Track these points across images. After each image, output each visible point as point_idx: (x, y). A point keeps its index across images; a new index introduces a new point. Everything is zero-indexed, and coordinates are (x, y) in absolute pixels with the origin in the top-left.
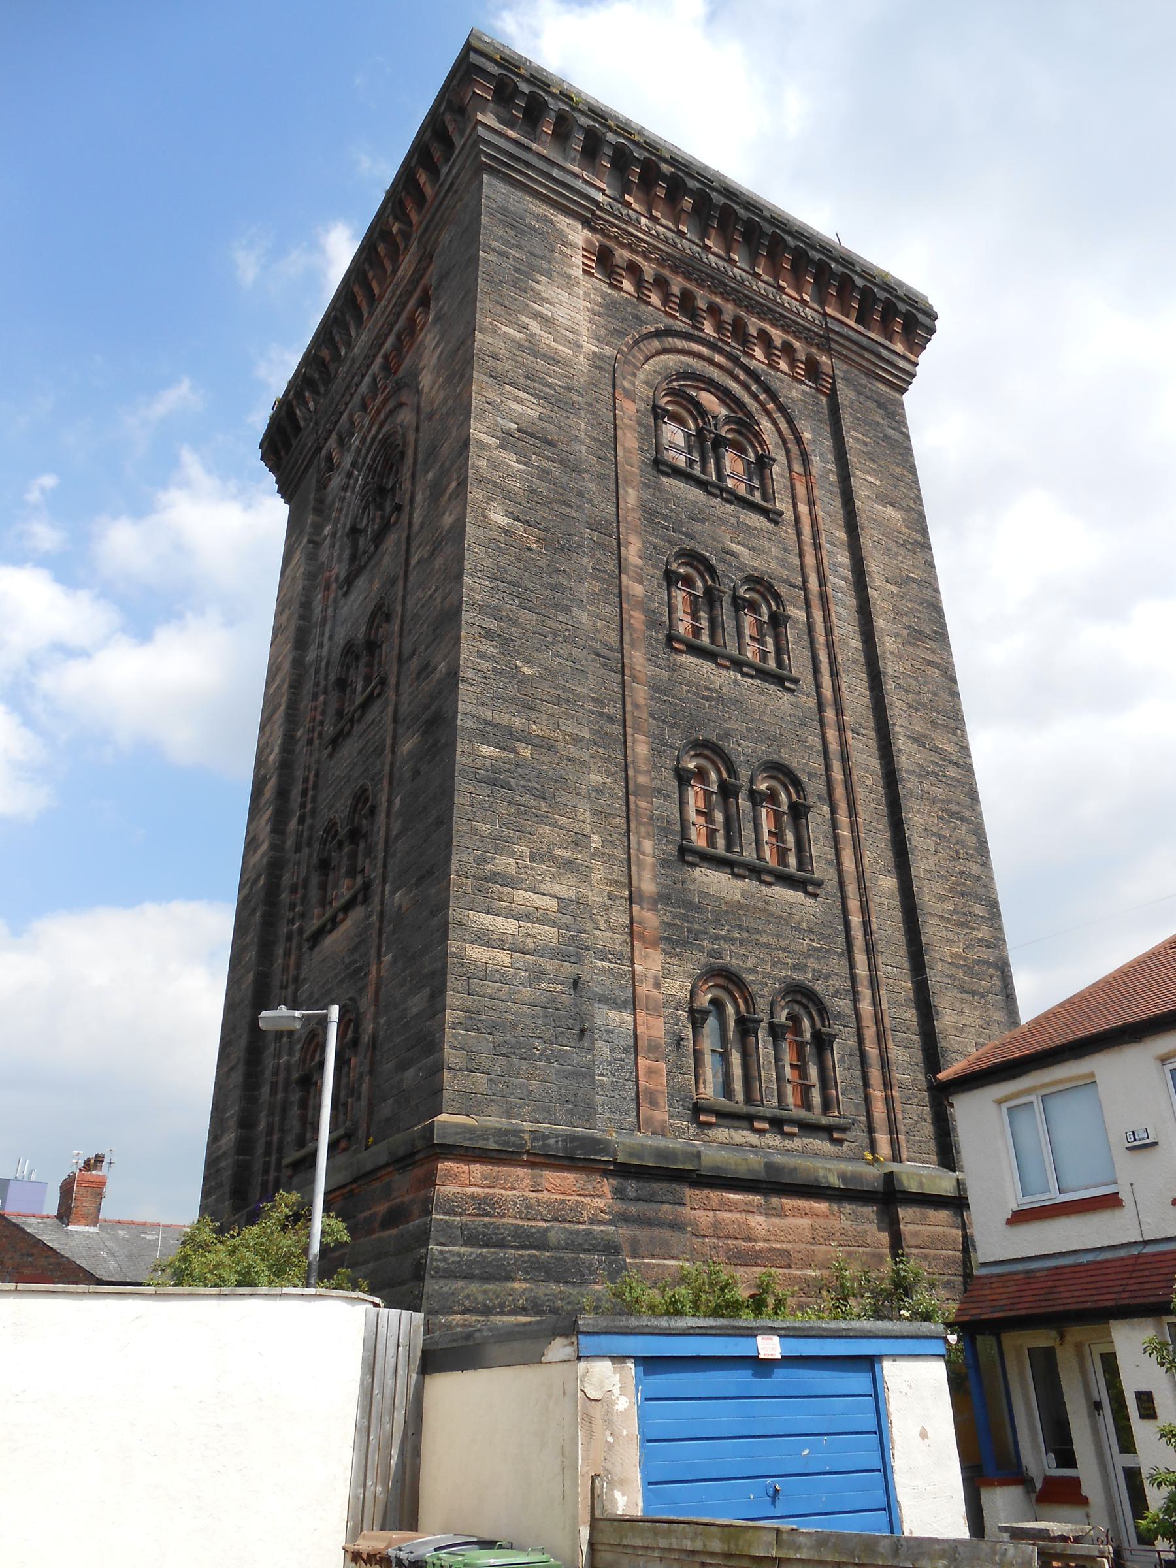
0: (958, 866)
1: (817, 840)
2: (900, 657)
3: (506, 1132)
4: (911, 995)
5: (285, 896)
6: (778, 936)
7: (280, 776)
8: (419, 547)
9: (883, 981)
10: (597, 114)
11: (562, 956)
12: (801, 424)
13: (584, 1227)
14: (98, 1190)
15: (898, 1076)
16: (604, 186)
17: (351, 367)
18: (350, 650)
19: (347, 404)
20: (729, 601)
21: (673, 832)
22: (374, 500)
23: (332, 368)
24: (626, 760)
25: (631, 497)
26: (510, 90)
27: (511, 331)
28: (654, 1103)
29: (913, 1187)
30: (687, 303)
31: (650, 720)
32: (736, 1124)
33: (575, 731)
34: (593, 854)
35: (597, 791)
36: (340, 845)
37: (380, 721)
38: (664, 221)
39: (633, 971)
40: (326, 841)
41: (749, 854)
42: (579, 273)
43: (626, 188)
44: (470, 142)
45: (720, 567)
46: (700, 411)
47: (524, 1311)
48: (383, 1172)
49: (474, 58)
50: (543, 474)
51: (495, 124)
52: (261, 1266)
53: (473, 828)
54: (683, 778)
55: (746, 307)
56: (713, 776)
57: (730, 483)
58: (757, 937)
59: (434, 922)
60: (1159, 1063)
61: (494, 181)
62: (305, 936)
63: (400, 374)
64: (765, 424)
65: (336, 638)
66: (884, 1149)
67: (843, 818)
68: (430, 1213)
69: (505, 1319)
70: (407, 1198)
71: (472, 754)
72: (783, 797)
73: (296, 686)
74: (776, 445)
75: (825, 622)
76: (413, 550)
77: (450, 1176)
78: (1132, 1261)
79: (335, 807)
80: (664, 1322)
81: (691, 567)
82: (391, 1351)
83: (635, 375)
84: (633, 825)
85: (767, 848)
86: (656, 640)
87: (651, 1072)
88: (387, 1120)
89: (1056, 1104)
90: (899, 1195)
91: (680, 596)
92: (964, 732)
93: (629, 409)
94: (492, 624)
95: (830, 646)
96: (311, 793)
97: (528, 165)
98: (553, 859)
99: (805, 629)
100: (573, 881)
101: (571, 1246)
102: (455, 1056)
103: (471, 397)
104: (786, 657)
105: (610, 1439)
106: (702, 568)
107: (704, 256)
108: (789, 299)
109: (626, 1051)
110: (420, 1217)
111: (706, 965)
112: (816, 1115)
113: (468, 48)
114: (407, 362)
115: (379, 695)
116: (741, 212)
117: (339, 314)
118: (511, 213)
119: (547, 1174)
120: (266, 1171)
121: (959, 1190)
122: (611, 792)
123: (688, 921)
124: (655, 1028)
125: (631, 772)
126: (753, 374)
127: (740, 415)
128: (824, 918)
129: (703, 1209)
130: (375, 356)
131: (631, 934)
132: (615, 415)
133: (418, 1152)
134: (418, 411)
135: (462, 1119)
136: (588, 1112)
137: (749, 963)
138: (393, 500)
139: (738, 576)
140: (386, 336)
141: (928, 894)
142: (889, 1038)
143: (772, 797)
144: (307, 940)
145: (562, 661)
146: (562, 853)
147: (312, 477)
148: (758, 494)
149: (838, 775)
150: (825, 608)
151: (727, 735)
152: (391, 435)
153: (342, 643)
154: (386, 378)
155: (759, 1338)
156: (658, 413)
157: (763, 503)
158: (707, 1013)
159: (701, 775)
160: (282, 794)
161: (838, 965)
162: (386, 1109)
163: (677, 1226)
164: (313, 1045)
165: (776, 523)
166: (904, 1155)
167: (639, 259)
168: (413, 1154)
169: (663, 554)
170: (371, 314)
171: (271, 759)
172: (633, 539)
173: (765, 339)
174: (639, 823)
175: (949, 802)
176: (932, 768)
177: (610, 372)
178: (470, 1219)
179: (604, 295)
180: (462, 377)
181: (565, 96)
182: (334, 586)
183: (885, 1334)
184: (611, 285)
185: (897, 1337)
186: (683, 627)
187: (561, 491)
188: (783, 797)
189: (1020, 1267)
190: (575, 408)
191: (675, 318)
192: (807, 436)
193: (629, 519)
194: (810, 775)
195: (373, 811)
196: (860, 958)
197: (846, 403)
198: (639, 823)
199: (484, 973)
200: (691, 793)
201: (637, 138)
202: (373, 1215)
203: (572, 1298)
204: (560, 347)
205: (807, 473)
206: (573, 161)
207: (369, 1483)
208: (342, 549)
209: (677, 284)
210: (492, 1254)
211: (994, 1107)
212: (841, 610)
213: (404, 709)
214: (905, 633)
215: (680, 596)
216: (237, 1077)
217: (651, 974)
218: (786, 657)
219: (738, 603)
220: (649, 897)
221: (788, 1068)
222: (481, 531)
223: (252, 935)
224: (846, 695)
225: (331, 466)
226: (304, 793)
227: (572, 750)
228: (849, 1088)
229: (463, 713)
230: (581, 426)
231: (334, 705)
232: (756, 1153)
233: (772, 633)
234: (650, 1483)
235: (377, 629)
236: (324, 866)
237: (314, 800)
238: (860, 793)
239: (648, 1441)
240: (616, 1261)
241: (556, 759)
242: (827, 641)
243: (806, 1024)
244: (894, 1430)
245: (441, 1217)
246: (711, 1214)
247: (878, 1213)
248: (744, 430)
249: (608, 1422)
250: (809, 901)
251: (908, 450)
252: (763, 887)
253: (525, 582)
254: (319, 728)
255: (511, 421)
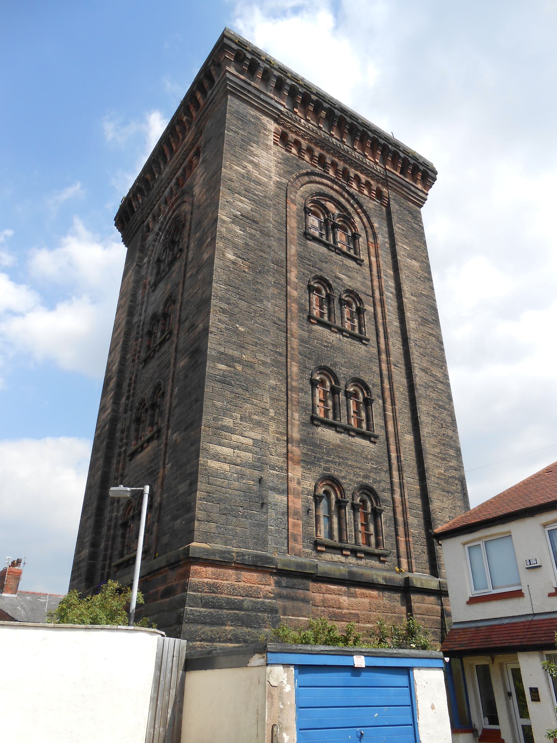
0: (442, 431)
1: (376, 416)
2: (417, 331)
3: (224, 552)
4: (419, 492)
5: (118, 435)
6: (357, 461)
7: (118, 377)
8: (191, 269)
9: (406, 485)
10: (283, 70)
11: (254, 467)
12: (373, 220)
13: (261, 600)
14: (17, 576)
15: (412, 531)
16: (285, 104)
17: (160, 183)
18: (155, 318)
19: (157, 201)
20: (338, 301)
21: (308, 410)
22: (169, 247)
23: (151, 183)
24: (287, 374)
25: (293, 250)
26: (241, 57)
27: (239, 169)
28: (296, 540)
29: (418, 585)
30: (321, 160)
31: (299, 355)
32: (335, 551)
33: (263, 359)
34: (270, 419)
35: (273, 388)
36: (147, 411)
37: (168, 352)
38: (312, 122)
39: (288, 476)
40: (139, 408)
41: (344, 422)
42: (271, 143)
43: (295, 105)
44: (223, 80)
45: (334, 285)
46: (326, 211)
47: (230, 641)
48: (163, 570)
49: (226, 41)
50: (252, 237)
51: (233, 72)
52: (102, 615)
53: (214, 405)
54: (314, 384)
55: (349, 164)
56: (328, 384)
57: (339, 245)
58: (347, 461)
59: (193, 448)
60: (542, 527)
61: (233, 99)
62: (127, 454)
63: (184, 187)
64: (357, 219)
65: (148, 312)
66: (405, 566)
67: (389, 406)
68: (186, 591)
69: (221, 644)
70: (175, 583)
71: (214, 368)
72: (361, 395)
73: (127, 334)
74: (361, 228)
75: (382, 313)
76: (188, 270)
77: (196, 573)
78: (528, 623)
79: (145, 392)
80: (300, 647)
81: (320, 284)
82: (170, 659)
83: (296, 192)
84: (289, 405)
85: (352, 419)
86: (303, 318)
87: (295, 525)
88: (166, 544)
89: (491, 546)
90: (411, 589)
91: (314, 298)
92: (446, 368)
93: (293, 208)
94: (226, 306)
95: (384, 324)
96: (133, 385)
97: (249, 92)
98: (251, 420)
99: (373, 316)
100: (260, 431)
101: (254, 609)
102: (201, 514)
103: (219, 198)
104: (363, 329)
105: (282, 707)
106: (325, 285)
107: (330, 139)
108: (369, 161)
109: (283, 514)
110: (181, 592)
111: (322, 474)
112: (372, 549)
113: (223, 36)
114: (188, 182)
115: (168, 339)
116: (348, 119)
117: (155, 158)
118: (240, 113)
119: (243, 573)
120: (103, 569)
121: (440, 587)
122: (280, 389)
123: (314, 453)
124: (297, 504)
125: (289, 380)
126: (351, 195)
127: (345, 214)
128: (378, 454)
129: (318, 593)
130: (172, 179)
131: (287, 458)
132: (286, 210)
133: (181, 561)
134: (192, 204)
135: (203, 545)
136: (265, 543)
137: (343, 474)
138: (178, 247)
139: (342, 289)
140: (178, 169)
141: (428, 444)
142: (408, 512)
143: (356, 395)
144: (129, 456)
145: (258, 326)
146: (255, 417)
147: (139, 235)
148: (352, 251)
149: (387, 386)
150: (383, 306)
151: (335, 364)
152: (178, 216)
153: (151, 314)
154: (177, 189)
155: (355, 657)
156: (307, 211)
157: (355, 255)
158: (322, 497)
159: (322, 383)
160: (119, 385)
161: (385, 476)
162: (165, 539)
163: (305, 601)
164: (130, 506)
165: (361, 265)
166: (414, 569)
167: (300, 139)
168: (179, 561)
169: (307, 277)
170: (171, 158)
171: (114, 368)
172: (293, 269)
173: (357, 179)
174: (293, 405)
175: (439, 400)
176: (431, 384)
177: (285, 190)
178: (206, 594)
179: (283, 155)
180: (215, 189)
181: (268, 61)
182: (148, 287)
183: (418, 656)
184: (286, 150)
185: (420, 658)
186: (316, 312)
187: (260, 245)
188: (361, 395)
189: (473, 625)
190: (268, 206)
191: (316, 167)
192: (376, 225)
193: (292, 260)
194: (374, 385)
195: (163, 394)
196: (395, 473)
197: (394, 211)
198: (293, 405)
199: (216, 474)
200: (317, 391)
201: (301, 83)
202: (157, 592)
203: (254, 635)
204: (261, 177)
205: (376, 243)
206: (270, 91)
207: (157, 726)
208: (153, 269)
209: (317, 151)
210: (216, 612)
211: (462, 546)
212: (390, 308)
213: (181, 346)
214: (420, 320)
215: (314, 298)
216: (91, 522)
217: (296, 477)
218: (363, 329)
219: (342, 302)
220: (297, 441)
221: (360, 525)
222: (222, 262)
223: (101, 453)
224: (391, 348)
225: (148, 230)
226: (130, 385)
227: (262, 368)
228: (388, 536)
229: (210, 348)
230: (271, 215)
231: (145, 343)
232: (344, 566)
233: (357, 317)
234: (300, 730)
235: (168, 308)
236: (138, 420)
237: (134, 389)
238: (397, 394)
239: (300, 708)
240: (276, 617)
241: (254, 372)
242: (383, 322)
243: (369, 504)
244: (419, 705)
245: (192, 593)
246: (322, 595)
247: (401, 597)
248: (347, 221)
249: (281, 698)
250: (372, 445)
251: (423, 235)
252: (350, 438)
253: (241, 287)
254: (138, 354)
255: (238, 210)
